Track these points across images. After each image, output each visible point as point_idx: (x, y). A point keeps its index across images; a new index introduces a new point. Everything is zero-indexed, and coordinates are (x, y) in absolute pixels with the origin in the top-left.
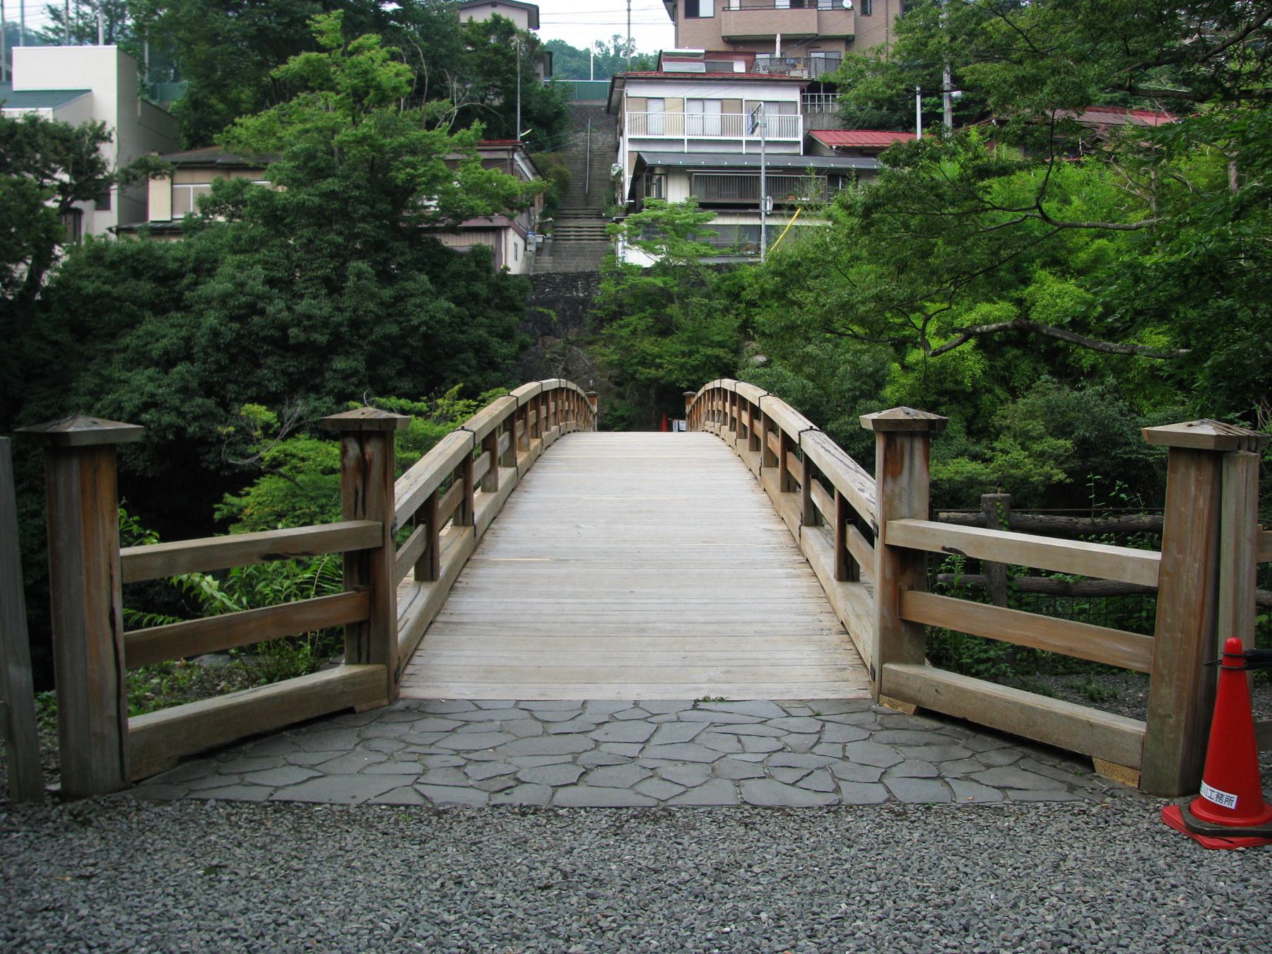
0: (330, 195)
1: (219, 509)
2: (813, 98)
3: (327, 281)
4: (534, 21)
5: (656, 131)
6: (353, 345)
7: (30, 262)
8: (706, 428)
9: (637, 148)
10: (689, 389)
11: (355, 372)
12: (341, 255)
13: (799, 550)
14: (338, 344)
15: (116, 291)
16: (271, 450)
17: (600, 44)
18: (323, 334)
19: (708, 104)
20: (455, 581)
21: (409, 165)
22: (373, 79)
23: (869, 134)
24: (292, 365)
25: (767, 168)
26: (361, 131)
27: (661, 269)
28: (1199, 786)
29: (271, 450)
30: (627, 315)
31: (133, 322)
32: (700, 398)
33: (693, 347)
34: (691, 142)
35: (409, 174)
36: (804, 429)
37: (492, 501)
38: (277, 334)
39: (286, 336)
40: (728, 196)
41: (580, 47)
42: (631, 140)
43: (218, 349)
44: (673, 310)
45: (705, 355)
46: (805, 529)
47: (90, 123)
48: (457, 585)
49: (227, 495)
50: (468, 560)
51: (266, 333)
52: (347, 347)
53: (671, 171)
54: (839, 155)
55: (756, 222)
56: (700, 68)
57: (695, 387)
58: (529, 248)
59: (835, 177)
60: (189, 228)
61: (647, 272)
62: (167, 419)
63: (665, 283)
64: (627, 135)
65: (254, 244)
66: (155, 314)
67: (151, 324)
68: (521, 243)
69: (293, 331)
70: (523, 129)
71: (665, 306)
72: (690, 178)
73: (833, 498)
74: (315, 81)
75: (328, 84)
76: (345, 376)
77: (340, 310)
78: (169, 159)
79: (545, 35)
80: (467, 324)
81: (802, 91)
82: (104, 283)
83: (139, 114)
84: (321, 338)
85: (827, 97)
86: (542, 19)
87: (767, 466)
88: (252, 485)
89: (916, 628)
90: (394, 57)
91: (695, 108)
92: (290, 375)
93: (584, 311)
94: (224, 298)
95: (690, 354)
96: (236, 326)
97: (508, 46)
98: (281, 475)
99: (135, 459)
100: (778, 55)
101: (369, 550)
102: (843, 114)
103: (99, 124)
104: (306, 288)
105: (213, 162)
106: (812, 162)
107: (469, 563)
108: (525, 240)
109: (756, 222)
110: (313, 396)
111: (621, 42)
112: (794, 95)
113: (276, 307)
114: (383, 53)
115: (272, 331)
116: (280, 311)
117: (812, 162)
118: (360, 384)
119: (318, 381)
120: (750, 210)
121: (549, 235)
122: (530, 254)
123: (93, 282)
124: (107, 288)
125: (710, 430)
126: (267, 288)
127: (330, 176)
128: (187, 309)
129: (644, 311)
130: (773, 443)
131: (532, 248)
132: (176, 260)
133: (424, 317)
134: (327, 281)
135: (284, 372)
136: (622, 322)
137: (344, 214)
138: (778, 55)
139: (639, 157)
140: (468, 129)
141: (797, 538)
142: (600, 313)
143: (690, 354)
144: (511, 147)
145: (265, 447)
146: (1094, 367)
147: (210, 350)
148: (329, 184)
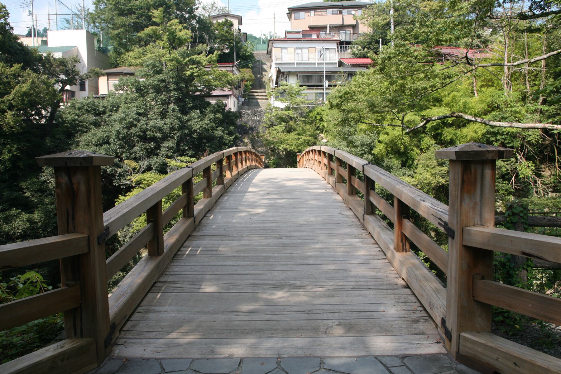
0: (162, 81)
1: (117, 201)
2: (341, 47)
4: (240, 23)
5: (285, 60)
6: (171, 138)
7: (49, 110)
8: (306, 166)
9: (277, 66)
10: (298, 152)
11: (172, 147)
12: (166, 103)
13: (364, 228)
14: (165, 138)
15: (81, 118)
16: (135, 178)
17: (265, 35)
19: (303, 50)
20: (179, 250)
21: (192, 69)
22: (176, 36)
24: (147, 146)
25: (326, 72)
27: (288, 109)
29: (135, 178)
30: (275, 125)
31: (88, 130)
32: (303, 155)
33: (299, 137)
34: (297, 63)
35: (191, 72)
36: (365, 163)
37: (209, 201)
38: (142, 134)
39: (146, 135)
40: (311, 82)
41: (258, 37)
42: (276, 64)
44: (291, 123)
45: (304, 139)
46: (366, 216)
47: (72, 56)
48: (180, 253)
49: (120, 196)
50: (189, 236)
51: (137, 134)
52: (169, 138)
53: (289, 73)
54: (351, 67)
55: (322, 91)
56: (300, 36)
57: (300, 151)
58: (239, 103)
59: (351, 74)
60: (111, 94)
61: (282, 109)
63: (289, 113)
64: (274, 61)
65: (132, 101)
66: (96, 127)
67: (94, 130)
68: (236, 101)
69: (148, 133)
70: (236, 61)
71: (289, 122)
72: (297, 76)
73: (392, 205)
74: (156, 37)
75: (159, 38)
76: (169, 149)
78: (104, 71)
79: (244, 29)
80: (215, 130)
81: (337, 45)
82: (76, 116)
83: (96, 55)
84: (159, 135)
85: (346, 47)
86: (243, 22)
87: (338, 182)
88: (131, 191)
89: (485, 307)
90: (185, 28)
92: (147, 149)
95: (298, 139)
96: (126, 130)
97: (231, 30)
98: (141, 187)
100: (328, 32)
101: (79, 256)
102: (351, 53)
103: (75, 56)
104: (153, 116)
105: (122, 73)
106: (342, 69)
107: (190, 238)
108: (238, 100)
109: (322, 91)
110: (155, 157)
111: (272, 34)
112: (335, 46)
114: (180, 27)
115: (140, 133)
117: (342, 69)
118: (174, 153)
119: (158, 151)
120: (319, 87)
121: (246, 98)
122: (240, 105)
123: (71, 115)
124: (77, 117)
125: (308, 167)
127: (161, 73)
129: (281, 124)
130: (342, 172)
131: (241, 103)
132: (103, 107)
133: (198, 126)
135: (145, 149)
136: (273, 129)
138: (328, 32)
139: (279, 69)
140: (213, 54)
141: (362, 220)
142: (265, 125)
143: (298, 139)
144: (232, 65)
145: (134, 177)
146: (451, 139)
147: (116, 140)
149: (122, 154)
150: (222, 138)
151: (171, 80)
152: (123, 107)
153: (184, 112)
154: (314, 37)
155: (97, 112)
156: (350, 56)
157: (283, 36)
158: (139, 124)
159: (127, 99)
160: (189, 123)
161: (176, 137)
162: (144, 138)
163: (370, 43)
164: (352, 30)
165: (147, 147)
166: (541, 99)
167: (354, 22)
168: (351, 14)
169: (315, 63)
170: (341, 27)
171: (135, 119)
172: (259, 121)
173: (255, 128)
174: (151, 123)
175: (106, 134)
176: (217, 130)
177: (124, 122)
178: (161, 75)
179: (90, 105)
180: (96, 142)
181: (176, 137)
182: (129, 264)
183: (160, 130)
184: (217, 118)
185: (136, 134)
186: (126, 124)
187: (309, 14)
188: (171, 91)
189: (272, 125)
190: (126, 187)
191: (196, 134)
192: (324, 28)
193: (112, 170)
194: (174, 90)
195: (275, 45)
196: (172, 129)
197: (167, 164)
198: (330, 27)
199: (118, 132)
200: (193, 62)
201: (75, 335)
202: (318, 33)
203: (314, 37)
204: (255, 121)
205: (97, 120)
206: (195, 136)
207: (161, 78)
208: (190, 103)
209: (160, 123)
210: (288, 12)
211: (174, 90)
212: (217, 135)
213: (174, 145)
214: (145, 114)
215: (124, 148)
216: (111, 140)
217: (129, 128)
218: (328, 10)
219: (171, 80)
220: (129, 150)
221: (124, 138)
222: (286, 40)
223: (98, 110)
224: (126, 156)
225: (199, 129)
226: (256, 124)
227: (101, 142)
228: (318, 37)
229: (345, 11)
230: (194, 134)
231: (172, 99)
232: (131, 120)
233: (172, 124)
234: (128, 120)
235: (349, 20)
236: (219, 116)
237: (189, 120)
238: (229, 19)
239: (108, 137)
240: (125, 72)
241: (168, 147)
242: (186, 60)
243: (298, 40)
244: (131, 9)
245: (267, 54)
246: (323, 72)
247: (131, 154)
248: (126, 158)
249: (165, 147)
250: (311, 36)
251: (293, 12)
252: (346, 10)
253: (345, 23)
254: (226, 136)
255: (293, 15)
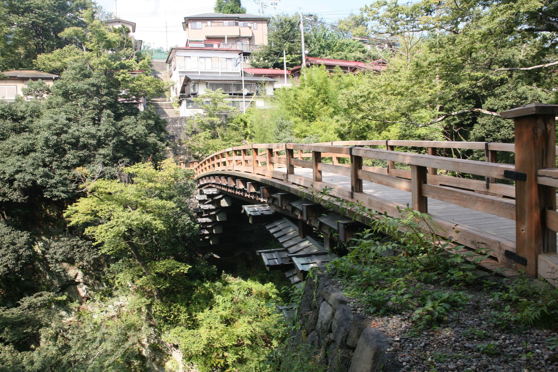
0: (93, 85)
3: (93, 119)
6: (106, 144)
11: (108, 155)
14: (100, 144)
18: (94, 140)
19: (207, 59)
23: (263, 70)
24: (81, 153)
25: (245, 81)
26: (102, 59)
28: (221, 274)
34: (201, 72)
38: (74, 141)
43: (48, 147)
51: (69, 141)
52: (103, 145)
56: (202, 45)
62: (28, 177)
64: (178, 70)
67: (13, 137)
77: (100, 130)
91: (202, 60)
92: (81, 157)
93: (181, 131)
94: (49, 126)
96: (55, 137)
99: (12, 195)
105: (16, 77)
113: (73, 129)
115: (72, 140)
116: (75, 131)
126: (67, 122)
128: (31, 131)
133: (134, 133)
134: (93, 119)
135: (78, 156)
137: (97, 93)
148: (91, 80)
149: (51, 163)
150: (155, 145)
151: (103, 84)
152: (47, 113)
153: (118, 117)
154: (216, 46)
155: (15, 117)
156: (250, 66)
157: (183, 45)
158: (70, 131)
159: (50, 103)
160: (123, 129)
161: (111, 144)
162: (75, 145)
163: (269, 55)
164: (248, 42)
165: (81, 155)
166: (438, 107)
167: (251, 35)
168: (247, 26)
169: (218, 73)
170: (238, 39)
171: (65, 125)
172: (180, 128)
173: (176, 136)
174: (84, 130)
175: (30, 142)
176: (150, 137)
177: (53, 128)
178: (91, 79)
179: (6, 110)
180: (20, 150)
181: (111, 144)
182: (53, 284)
183: (93, 136)
184: (149, 124)
185: (67, 141)
186: (55, 130)
187: (206, 24)
188: (103, 96)
189: (195, 132)
190: (59, 199)
191: (131, 141)
192: (221, 39)
193: (42, 180)
194: (106, 94)
195: (179, 53)
196: (107, 136)
197: (34, 182)
198: (228, 38)
199: (47, 140)
200: (123, 67)
201: (544, 250)
202: (219, 43)
203: (216, 46)
204: (176, 129)
205: (15, 126)
206: (130, 142)
207: (92, 82)
208: (122, 109)
209: (93, 130)
210: (184, 21)
211: (106, 94)
212: (150, 142)
213: (110, 152)
214: (76, 121)
215: (54, 156)
216: (38, 147)
217: (58, 135)
218: (224, 22)
219: (103, 84)
220: (61, 158)
221: (55, 145)
222: (187, 49)
223: (16, 115)
224: (57, 165)
225: (135, 135)
226: (178, 132)
227: (25, 150)
228: (219, 46)
229: (240, 23)
230: (129, 140)
231: (104, 104)
232: (61, 126)
233: (107, 130)
234: (57, 126)
235: (246, 32)
236: (151, 122)
237: (122, 127)
238: (126, 26)
239: (33, 144)
240: (18, 76)
241: (103, 155)
242: (116, 64)
243: (201, 49)
244: (29, 7)
245: (166, 62)
246: (241, 81)
247: (62, 162)
248: (56, 167)
249: (100, 154)
250: (212, 45)
251: (189, 22)
252: (242, 23)
253: (242, 35)
254: (159, 143)
255: (189, 25)
